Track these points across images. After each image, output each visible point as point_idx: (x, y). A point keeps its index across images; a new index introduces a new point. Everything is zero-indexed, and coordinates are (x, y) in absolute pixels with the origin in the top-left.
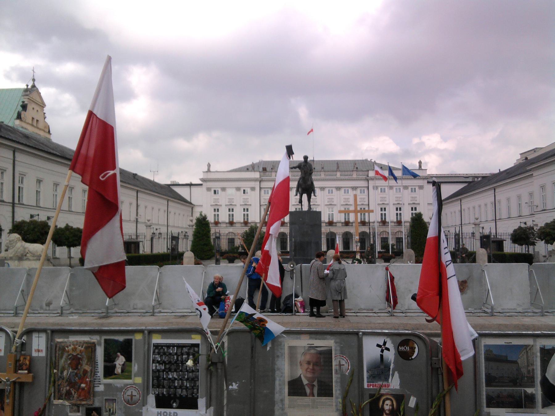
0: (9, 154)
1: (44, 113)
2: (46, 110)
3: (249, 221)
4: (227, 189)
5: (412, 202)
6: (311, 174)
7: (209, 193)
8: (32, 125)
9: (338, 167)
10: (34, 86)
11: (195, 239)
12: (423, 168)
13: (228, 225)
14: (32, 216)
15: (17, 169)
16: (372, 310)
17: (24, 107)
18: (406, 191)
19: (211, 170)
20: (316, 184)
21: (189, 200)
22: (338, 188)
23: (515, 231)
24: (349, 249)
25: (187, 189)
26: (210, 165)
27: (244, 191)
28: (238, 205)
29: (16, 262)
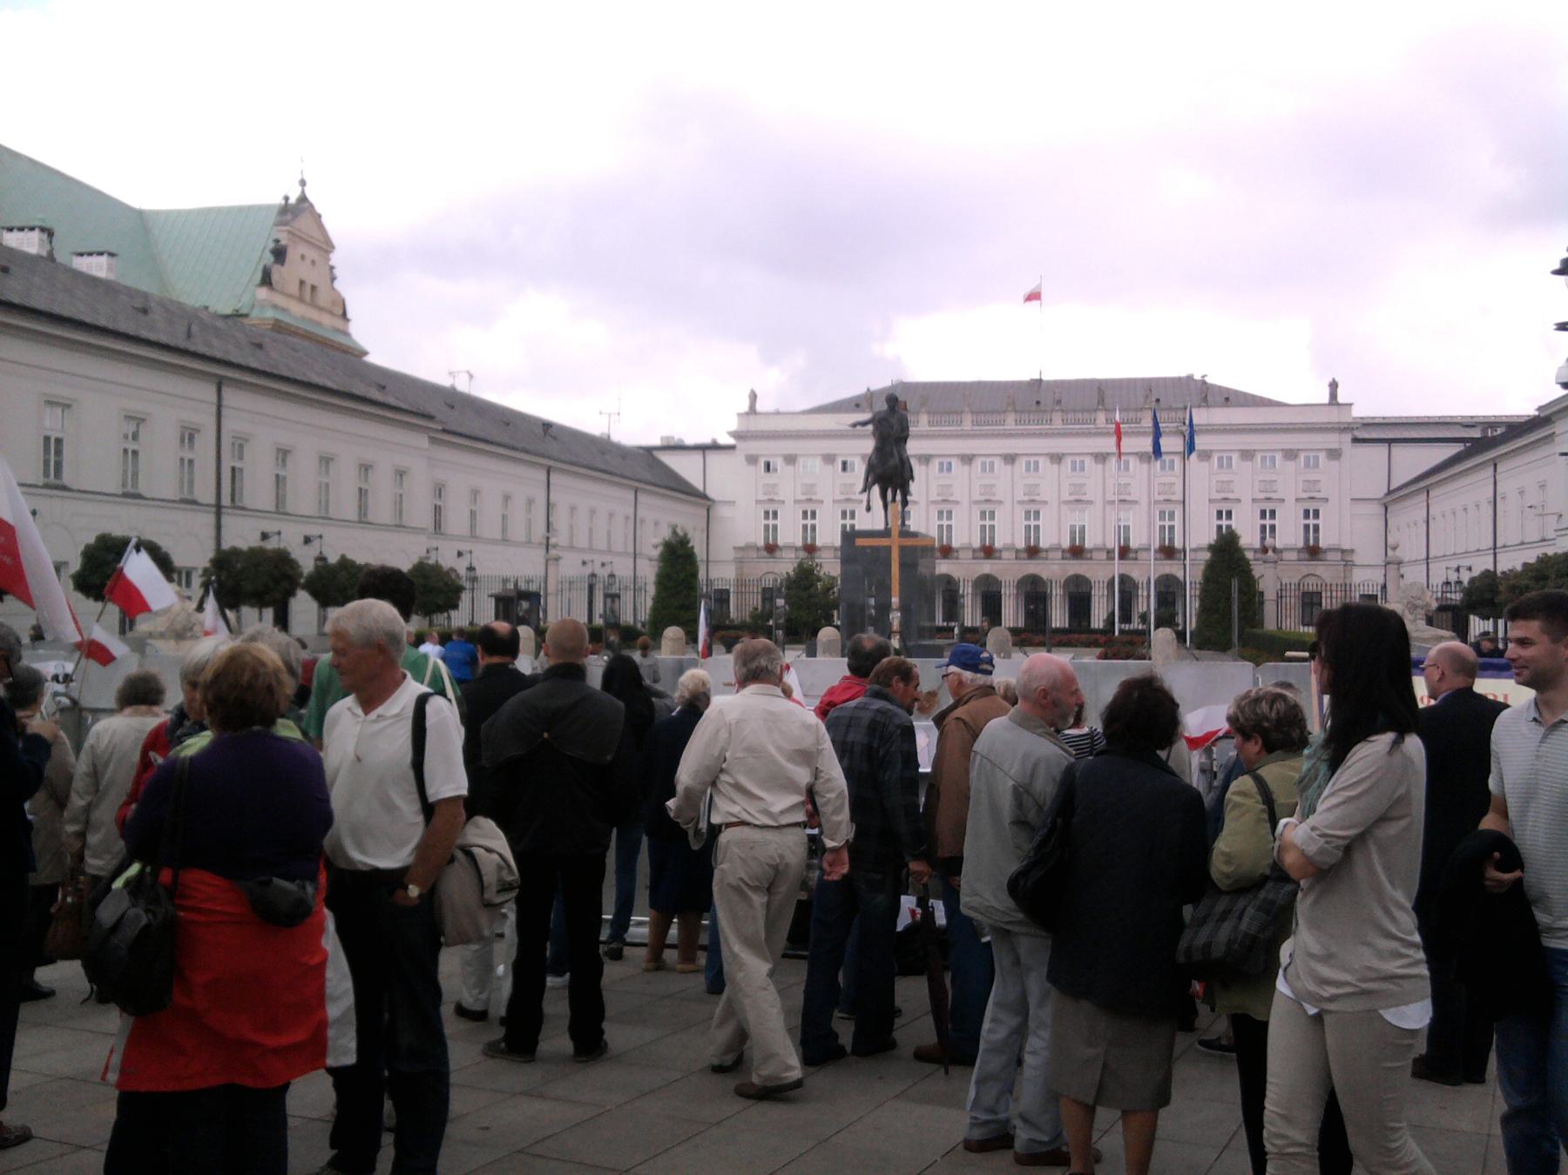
0: (208, 392)
1: (332, 268)
2: (335, 259)
3: (997, 545)
4: (801, 461)
6: (905, 440)
7: (752, 468)
8: (301, 300)
9: (1101, 401)
10: (303, 199)
11: (658, 592)
12: (1340, 400)
14: (265, 536)
15: (227, 425)
17: (280, 254)
18: (1291, 465)
19: (759, 407)
25: (697, 457)
27: (844, 464)
28: (828, 501)
29: (172, 643)
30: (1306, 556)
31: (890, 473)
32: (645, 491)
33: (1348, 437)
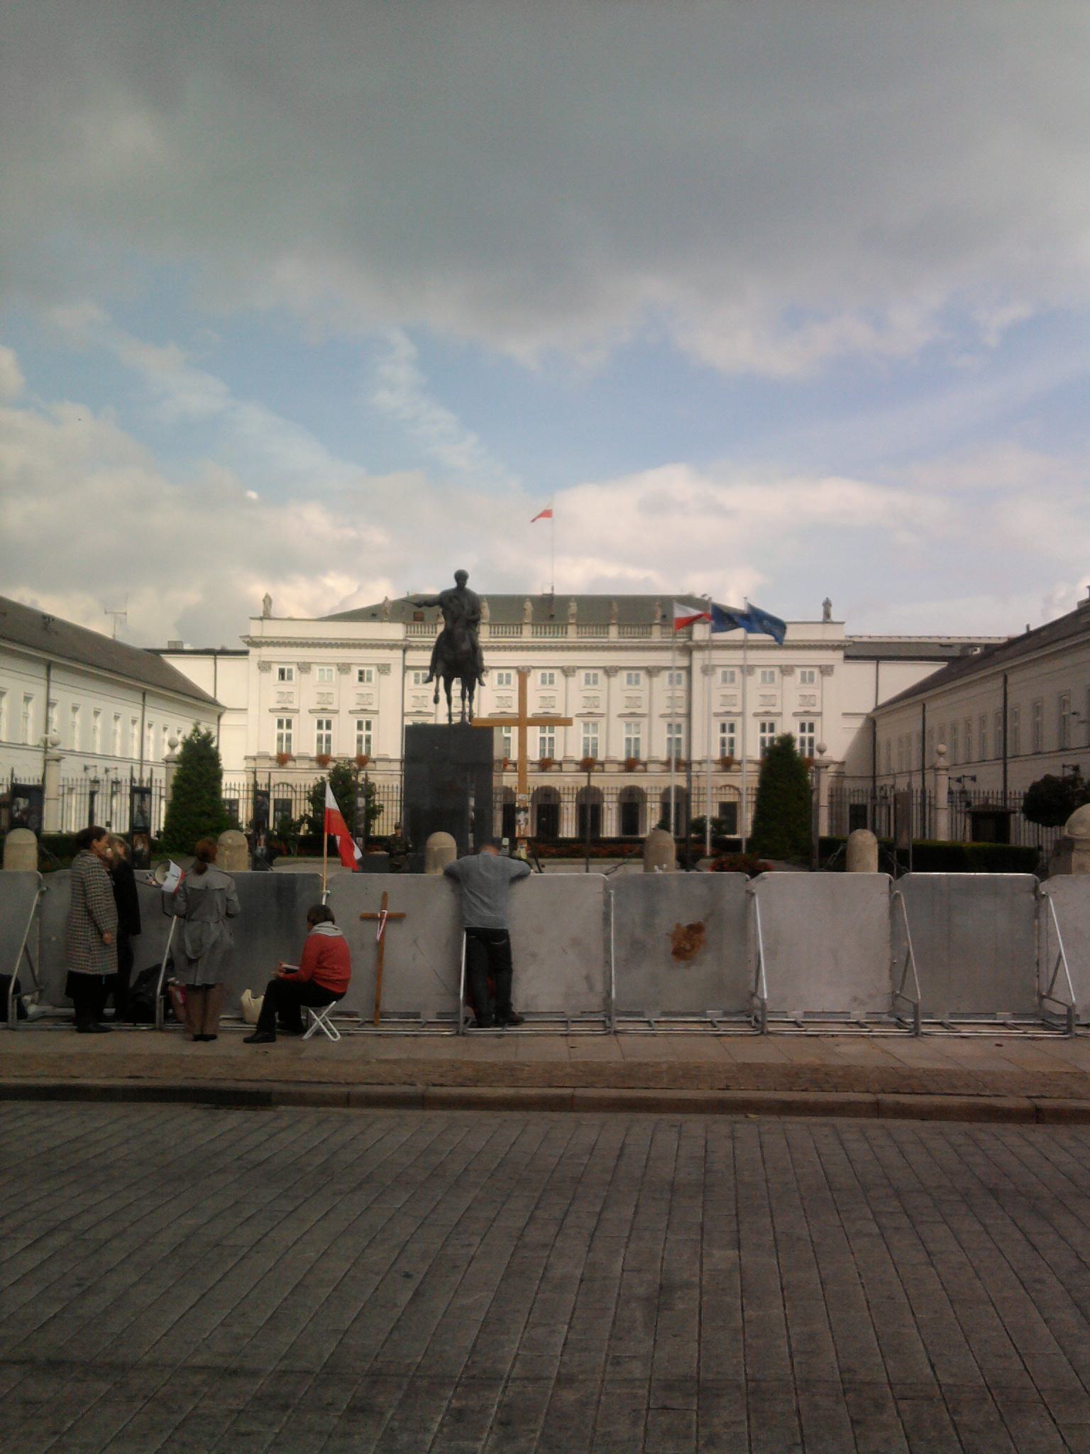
3: (373, 755)
5: (801, 710)
12: (834, 617)
13: (314, 764)
16: (417, 1015)
18: (787, 679)
20: (488, 658)
21: (211, 694)
22: (567, 672)
23: (1034, 787)
24: (1007, 840)
25: (206, 663)
26: (270, 602)
28: (304, 712)
30: (719, 767)
31: (457, 663)
32: (153, 694)
33: (840, 654)
